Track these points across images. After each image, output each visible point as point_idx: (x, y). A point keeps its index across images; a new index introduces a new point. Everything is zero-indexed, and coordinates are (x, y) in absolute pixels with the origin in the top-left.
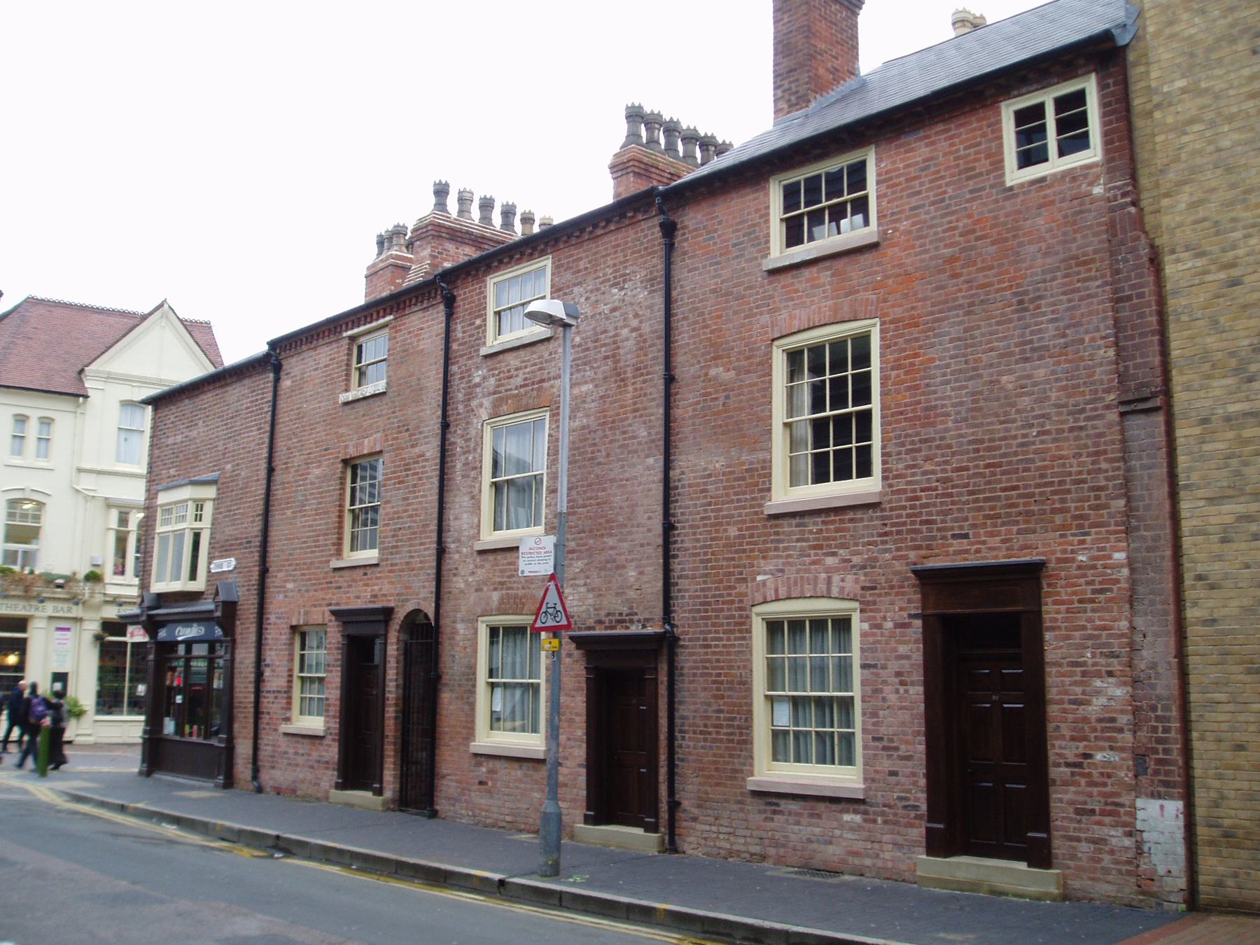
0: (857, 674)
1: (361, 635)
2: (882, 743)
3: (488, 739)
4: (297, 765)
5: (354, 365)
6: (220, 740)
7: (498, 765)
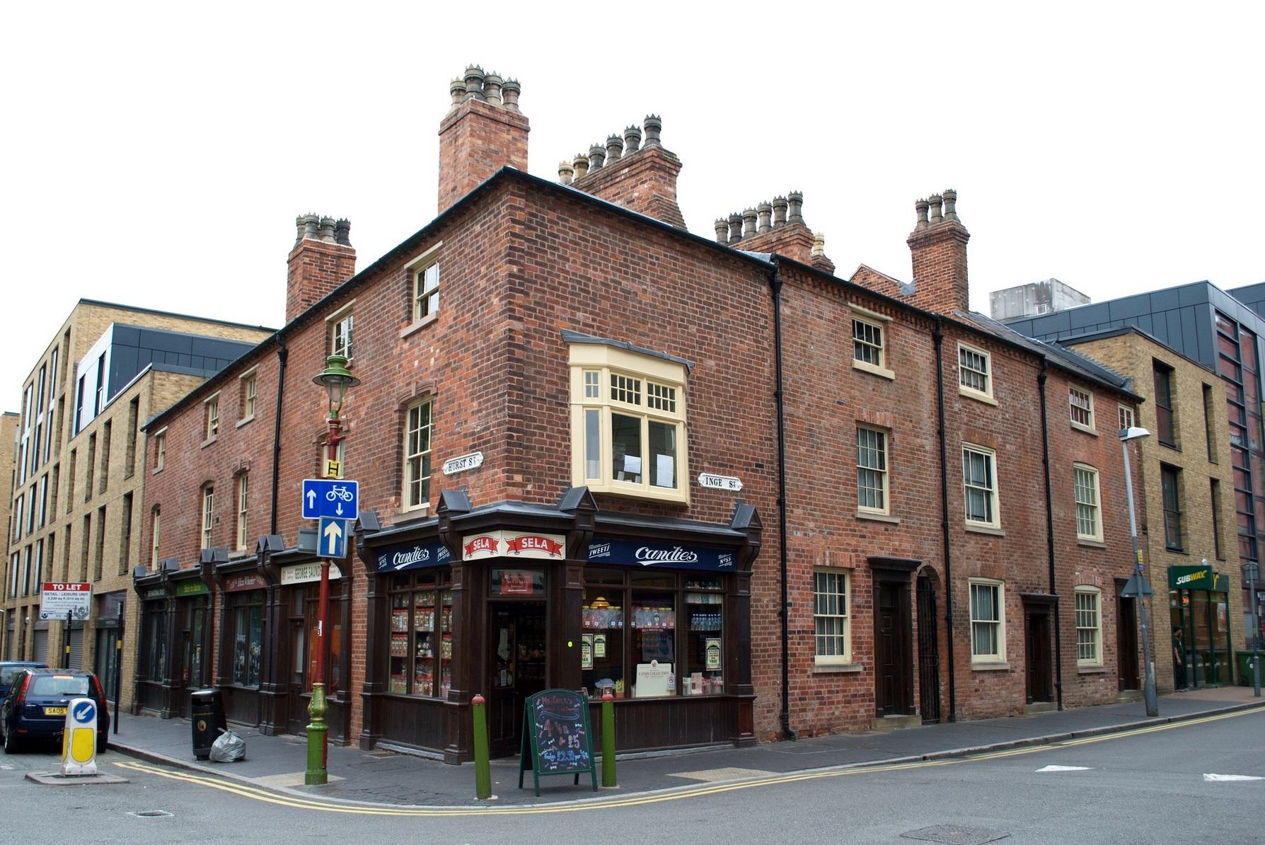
1: (889, 578)
2: (857, 643)
4: (833, 703)
5: (416, 297)
6: (339, 697)
7: (986, 676)
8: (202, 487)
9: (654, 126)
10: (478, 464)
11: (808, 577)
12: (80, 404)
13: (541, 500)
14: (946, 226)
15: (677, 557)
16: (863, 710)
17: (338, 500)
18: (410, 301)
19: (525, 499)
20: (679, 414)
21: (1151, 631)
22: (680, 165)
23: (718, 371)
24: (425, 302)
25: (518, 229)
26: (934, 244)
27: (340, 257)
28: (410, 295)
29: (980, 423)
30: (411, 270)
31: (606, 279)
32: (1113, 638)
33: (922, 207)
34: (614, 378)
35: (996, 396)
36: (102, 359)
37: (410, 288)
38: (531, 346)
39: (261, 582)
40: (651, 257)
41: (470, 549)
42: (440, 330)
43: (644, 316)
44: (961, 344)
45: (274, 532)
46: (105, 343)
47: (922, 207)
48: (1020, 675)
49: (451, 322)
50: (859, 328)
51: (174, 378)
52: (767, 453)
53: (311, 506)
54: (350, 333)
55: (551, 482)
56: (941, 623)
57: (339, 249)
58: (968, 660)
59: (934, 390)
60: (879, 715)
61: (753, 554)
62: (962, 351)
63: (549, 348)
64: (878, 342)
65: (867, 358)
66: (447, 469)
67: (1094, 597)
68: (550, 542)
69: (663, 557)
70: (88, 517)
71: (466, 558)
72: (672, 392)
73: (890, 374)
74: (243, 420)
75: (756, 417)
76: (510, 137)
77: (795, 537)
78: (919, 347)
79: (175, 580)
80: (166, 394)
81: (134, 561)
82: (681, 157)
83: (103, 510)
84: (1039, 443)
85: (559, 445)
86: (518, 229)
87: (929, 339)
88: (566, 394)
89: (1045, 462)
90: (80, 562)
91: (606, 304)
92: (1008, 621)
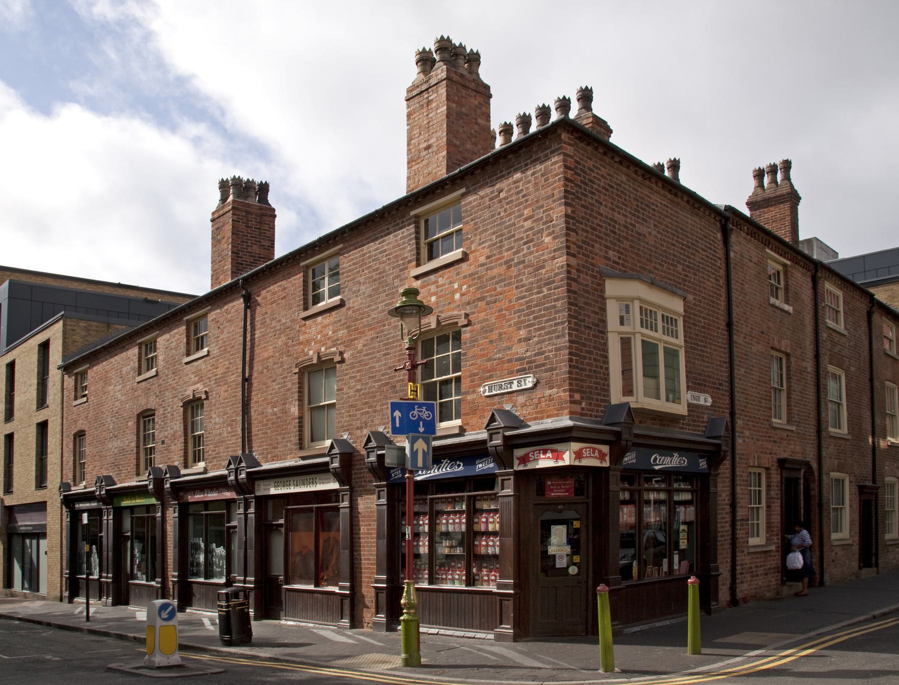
9: (586, 96)
10: (530, 385)
13: (591, 416)
14: (785, 190)
17: (420, 418)
19: (582, 415)
22: (611, 131)
23: (695, 304)
26: (772, 206)
27: (262, 215)
29: (837, 350)
31: (626, 222)
33: (759, 175)
35: (846, 328)
38: (580, 280)
40: (653, 204)
43: (651, 255)
47: (759, 175)
48: (856, 548)
49: (482, 259)
51: (82, 324)
52: (724, 376)
53: (398, 425)
55: (597, 400)
57: (261, 209)
58: (830, 536)
63: (592, 283)
66: (484, 390)
68: (600, 452)
75: (717, 341)
76: (476, 102)
80: (77, 338)
85: (601, 367)
87: (809, 280)
88: (604, 322)
91: (626, 244)
92: (851, 506)
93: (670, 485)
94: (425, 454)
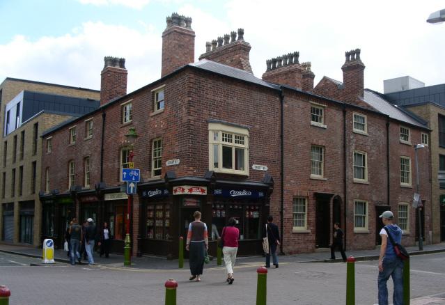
0: (408, 214)
1: (322, 201)
3: (357, 229)
5: (155, 102)
8: (69, 162)
9: (241, 32)
11: (291, 200)
12: (8, 122)
15: (244, 193)
16: (311, 246)
18: (153, 103)
20: (246, 145)
21: (431, 220)
24: (159, 104)
25: (191, 85)
27: (121, 73)
28: (154, 101)
30: (154, 92)
32: (414, 222)
33: (348, 55)
34: (223, 134)
35: (368, 132)
36: (18, 105)
37: (153, 99)
39: (96, 199)
41: (176, 191)
42: (164, 116)
44: (354, 113)
45: (102, 181)
46: (20, 98)
47: (348, 55)
50: (314, 110)
51: (52, 116)
52: (277, 157)
54: (130, 111)
56: (342, 216)
58: (353, 229)
59: (342, 131)
60: (317, 247)
61: (271, 192)
62: (355, 116)
64: (321, 114)
65: (317, 121)
67: (407, 207)
69: (239, 194)
70: (14, 170)
71: (174, 194)
72: (243, 138)
73: (326, 126)
74: (89, 136)
75: (275, 144)
77: (287, 186)
78: (337, 116)
79: (56, 197)
81: (38, 190)
82: (251, 45)
83: (21, 168)
84: (386, 148)
86: (191, 85)
87: (341, 112)
88: (207, 140)
89: (388, 156)
90: (11, 188)
93: (155, 207)
94: (134, 188)
